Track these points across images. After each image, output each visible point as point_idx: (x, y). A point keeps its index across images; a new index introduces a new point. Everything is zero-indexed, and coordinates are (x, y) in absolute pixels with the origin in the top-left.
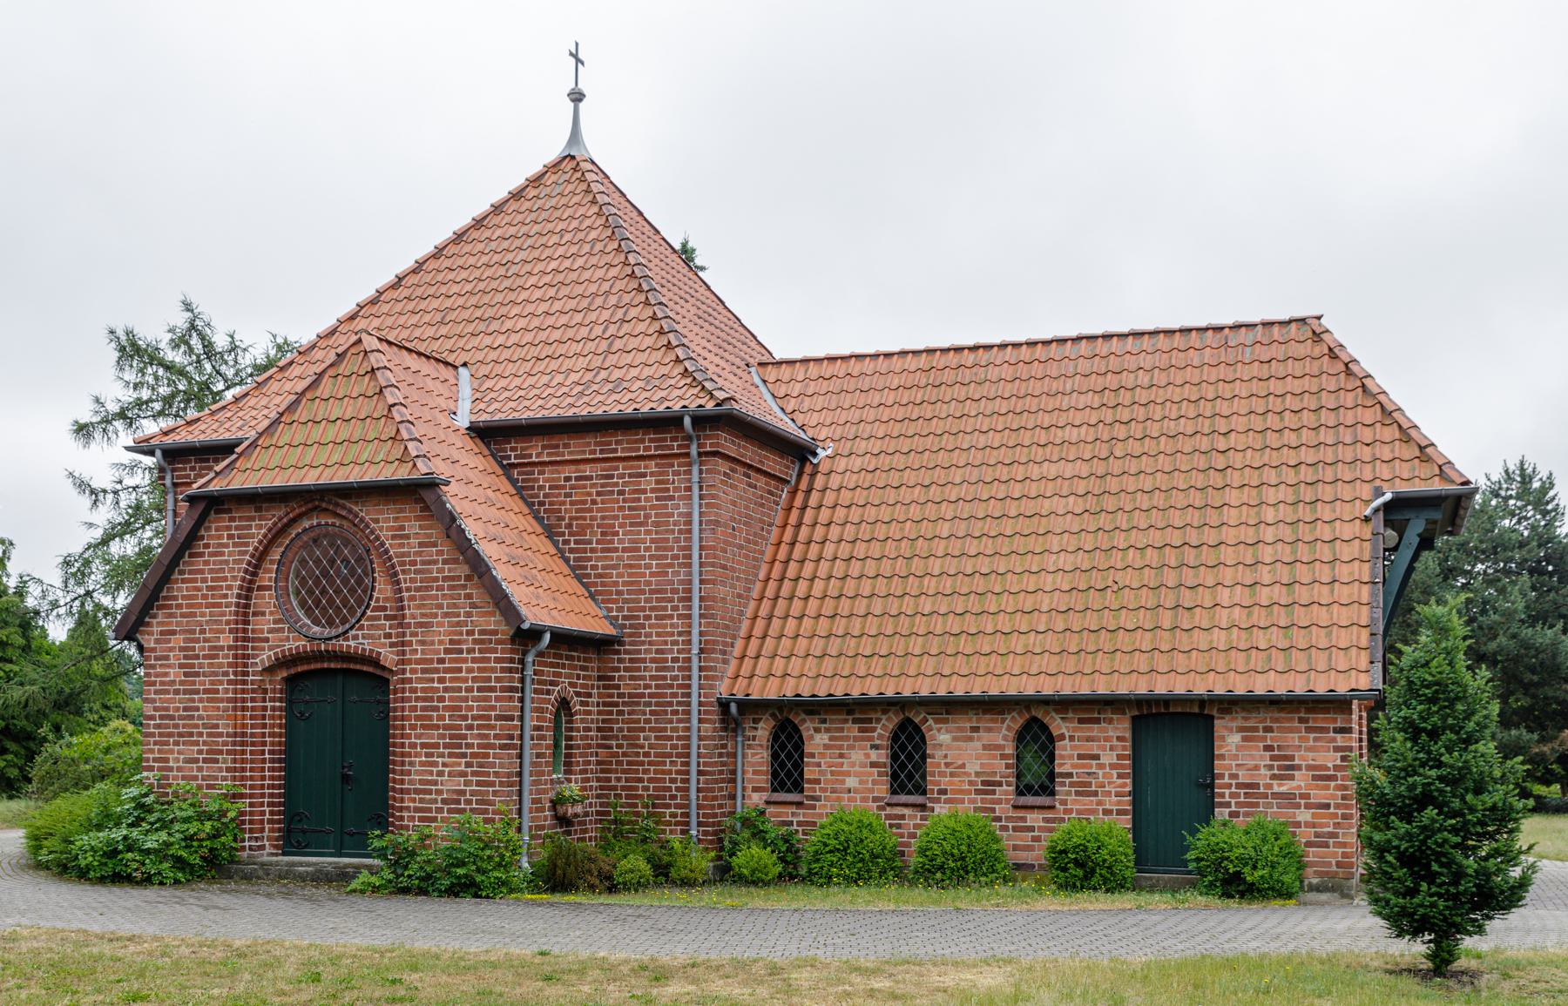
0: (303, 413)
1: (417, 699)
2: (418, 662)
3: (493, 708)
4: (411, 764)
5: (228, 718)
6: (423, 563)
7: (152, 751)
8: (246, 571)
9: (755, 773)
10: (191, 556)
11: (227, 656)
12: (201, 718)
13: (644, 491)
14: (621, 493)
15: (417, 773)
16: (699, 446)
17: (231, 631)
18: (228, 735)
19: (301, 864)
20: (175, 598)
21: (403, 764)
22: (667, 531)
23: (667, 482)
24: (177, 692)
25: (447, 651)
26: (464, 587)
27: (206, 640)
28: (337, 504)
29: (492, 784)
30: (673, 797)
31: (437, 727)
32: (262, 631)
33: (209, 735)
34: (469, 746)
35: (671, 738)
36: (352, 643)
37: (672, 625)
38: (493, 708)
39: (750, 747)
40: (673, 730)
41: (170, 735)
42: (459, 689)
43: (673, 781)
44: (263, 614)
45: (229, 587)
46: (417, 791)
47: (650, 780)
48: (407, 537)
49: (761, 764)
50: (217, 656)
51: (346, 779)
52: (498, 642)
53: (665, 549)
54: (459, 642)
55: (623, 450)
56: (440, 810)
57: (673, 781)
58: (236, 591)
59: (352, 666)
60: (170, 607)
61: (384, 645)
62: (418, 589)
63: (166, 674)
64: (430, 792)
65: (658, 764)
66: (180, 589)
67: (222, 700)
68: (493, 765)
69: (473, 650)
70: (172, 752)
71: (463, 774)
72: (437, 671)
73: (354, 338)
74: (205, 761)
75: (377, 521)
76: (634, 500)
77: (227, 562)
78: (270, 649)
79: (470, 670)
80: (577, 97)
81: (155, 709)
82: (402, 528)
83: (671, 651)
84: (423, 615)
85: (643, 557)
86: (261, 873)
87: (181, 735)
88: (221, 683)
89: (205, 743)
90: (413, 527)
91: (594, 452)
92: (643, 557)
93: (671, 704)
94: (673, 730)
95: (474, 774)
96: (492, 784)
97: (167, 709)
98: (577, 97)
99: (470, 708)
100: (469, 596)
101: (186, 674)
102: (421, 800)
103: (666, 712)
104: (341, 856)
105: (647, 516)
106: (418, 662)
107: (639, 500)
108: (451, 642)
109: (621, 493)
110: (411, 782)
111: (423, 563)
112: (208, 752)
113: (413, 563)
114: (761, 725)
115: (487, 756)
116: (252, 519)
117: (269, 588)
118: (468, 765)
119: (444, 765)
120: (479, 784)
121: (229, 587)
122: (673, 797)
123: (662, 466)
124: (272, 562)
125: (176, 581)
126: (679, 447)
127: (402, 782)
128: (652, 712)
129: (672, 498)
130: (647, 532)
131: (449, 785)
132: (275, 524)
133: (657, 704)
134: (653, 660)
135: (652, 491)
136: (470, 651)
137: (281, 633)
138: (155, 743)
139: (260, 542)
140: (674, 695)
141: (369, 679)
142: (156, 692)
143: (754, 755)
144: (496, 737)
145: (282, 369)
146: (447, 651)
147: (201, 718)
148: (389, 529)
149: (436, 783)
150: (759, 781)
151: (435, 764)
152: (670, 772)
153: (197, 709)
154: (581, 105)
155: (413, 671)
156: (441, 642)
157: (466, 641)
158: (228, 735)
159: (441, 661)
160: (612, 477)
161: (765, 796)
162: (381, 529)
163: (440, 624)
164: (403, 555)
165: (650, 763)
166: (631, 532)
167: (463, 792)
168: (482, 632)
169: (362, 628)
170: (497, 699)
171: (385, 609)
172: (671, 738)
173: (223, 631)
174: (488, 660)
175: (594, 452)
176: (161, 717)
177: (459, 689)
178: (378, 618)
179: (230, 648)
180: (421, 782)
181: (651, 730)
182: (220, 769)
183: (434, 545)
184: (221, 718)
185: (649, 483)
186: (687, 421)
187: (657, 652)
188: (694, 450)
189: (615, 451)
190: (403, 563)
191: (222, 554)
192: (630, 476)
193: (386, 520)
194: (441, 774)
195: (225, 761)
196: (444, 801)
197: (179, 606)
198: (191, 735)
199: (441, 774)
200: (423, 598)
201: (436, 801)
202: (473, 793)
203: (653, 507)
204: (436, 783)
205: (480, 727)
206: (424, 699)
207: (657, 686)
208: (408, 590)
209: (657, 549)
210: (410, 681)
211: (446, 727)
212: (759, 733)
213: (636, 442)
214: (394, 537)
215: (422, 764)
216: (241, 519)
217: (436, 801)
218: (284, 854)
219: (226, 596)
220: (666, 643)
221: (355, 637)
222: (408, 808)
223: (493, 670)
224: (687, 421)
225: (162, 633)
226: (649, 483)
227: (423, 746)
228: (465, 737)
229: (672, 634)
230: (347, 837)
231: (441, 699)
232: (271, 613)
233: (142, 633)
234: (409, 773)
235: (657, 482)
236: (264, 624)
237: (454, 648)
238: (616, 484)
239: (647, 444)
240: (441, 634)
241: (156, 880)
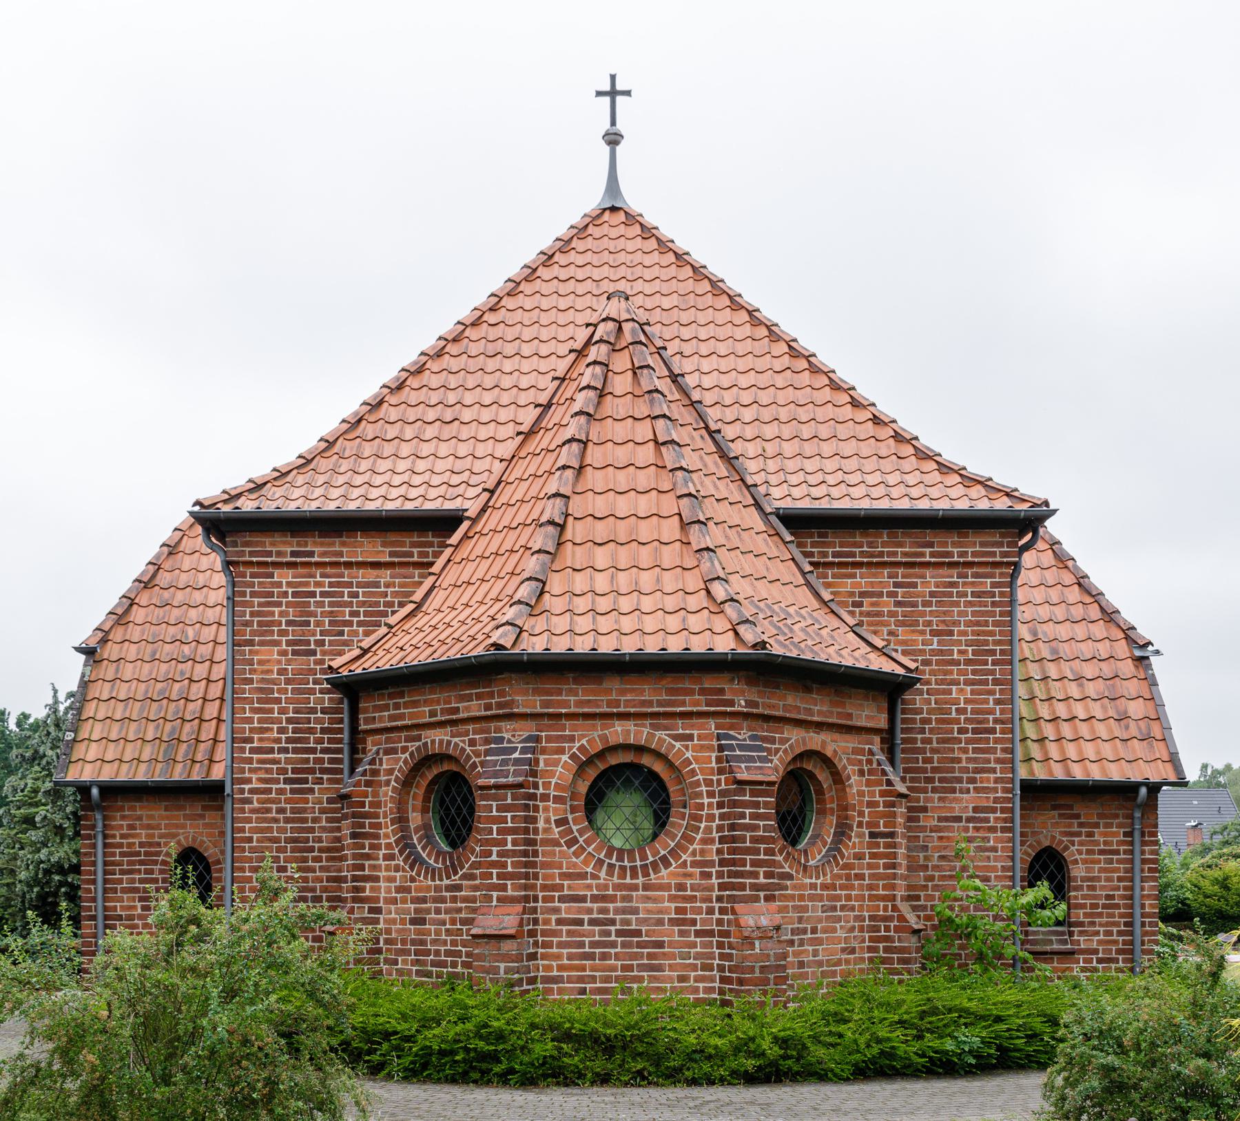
154: (618, 148)
239: (368, 548)
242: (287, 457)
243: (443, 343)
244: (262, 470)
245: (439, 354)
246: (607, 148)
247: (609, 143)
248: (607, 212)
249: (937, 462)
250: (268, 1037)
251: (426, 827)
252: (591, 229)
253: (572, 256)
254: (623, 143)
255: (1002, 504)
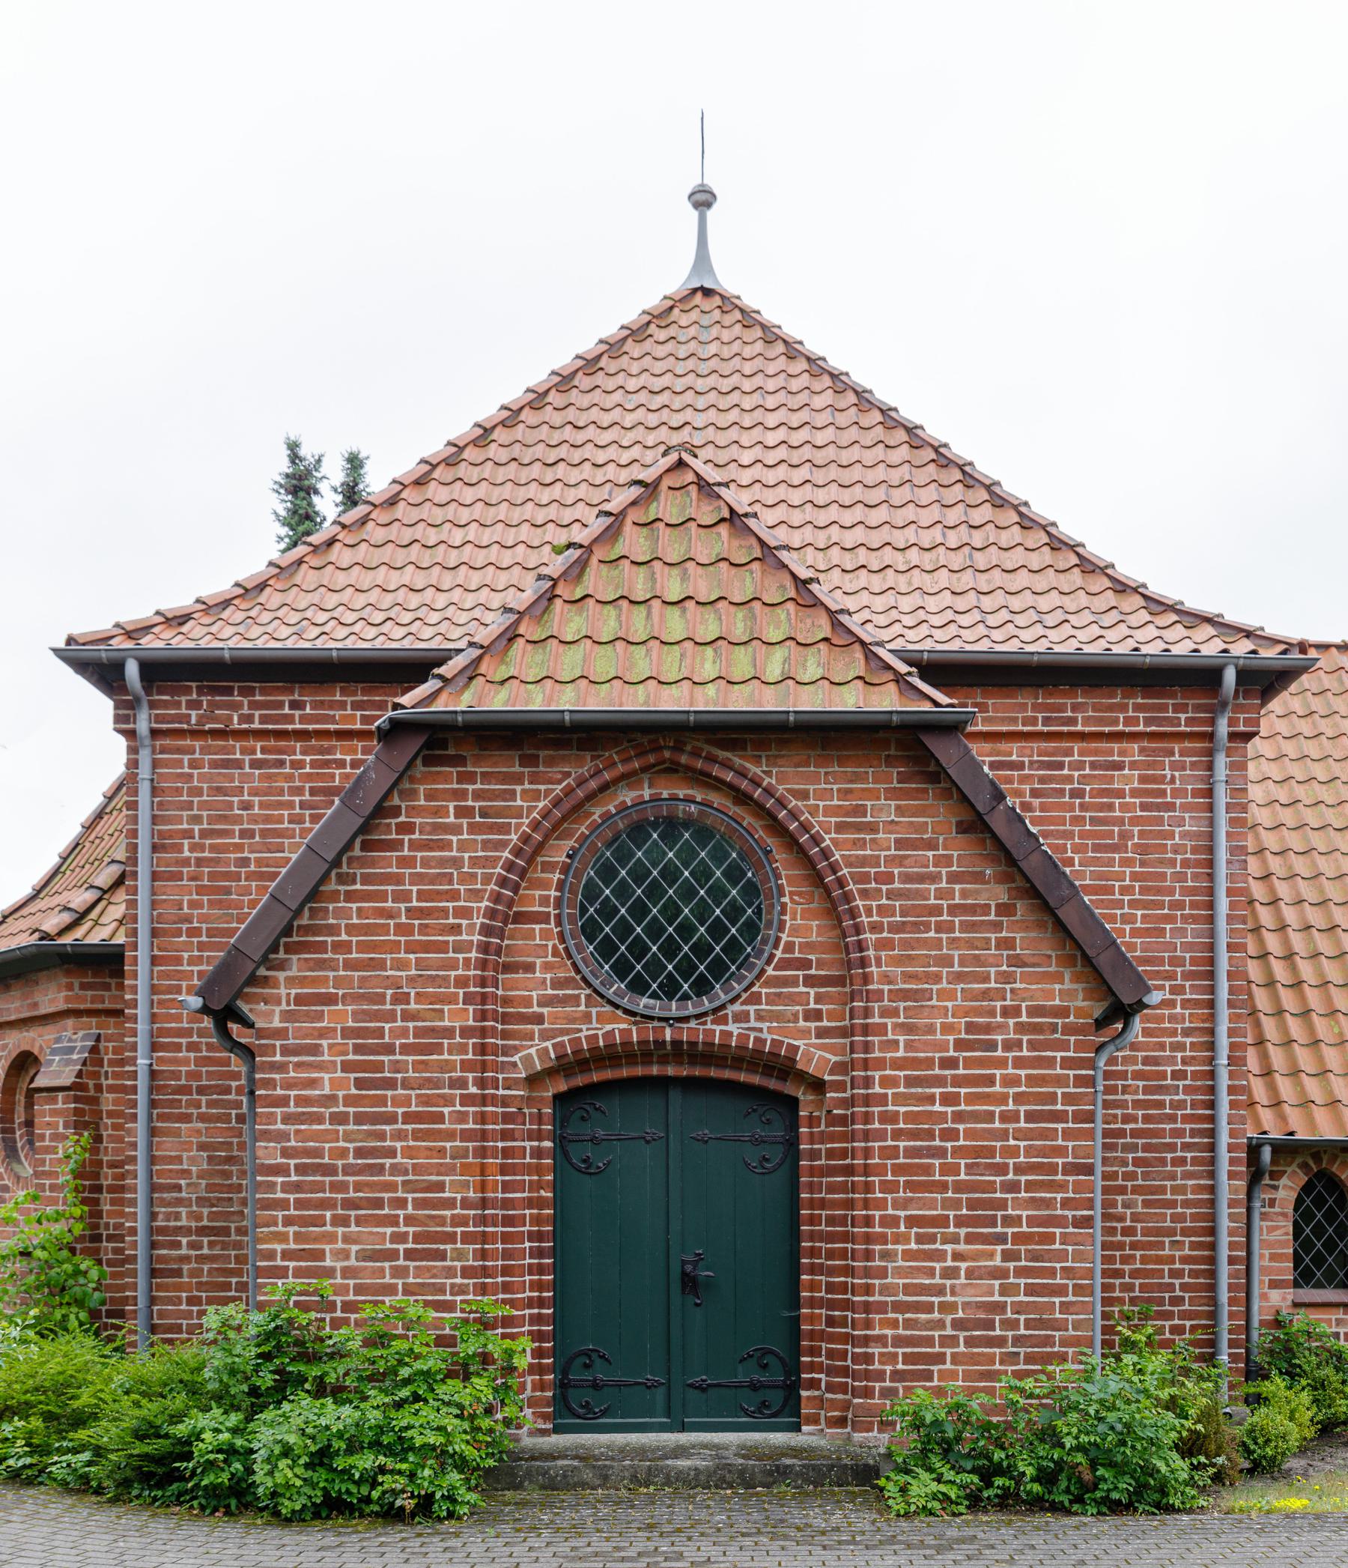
0: (597, 580)
1: (897, 1135)
2: (897, 1064)
3: (1061, 1151)
4: (886, 1255)
5: (466, 1169)
6: (907, 878)
7: (282, 1238)
8: (503, 882)
9: (1273, 1257)
10: (366, 846)
11: (462, 1049)
12: (396, 1169)
13: (1120, 793)
14: (1077, 793)
15: (899, 1272)
16: (1232, 722)
17: (468, 999)
18: (466, 1204)
19: (680, 1452)
20: (333, 930)
21: (868, 1255)
22: (1162, 862)
23: (1161, 779)
24: (340, 1119)
25: (960, 1045)
26: (997, 926)
27: (407, 1016)
28: (712, 759)
29: (1061, 1291)
30: (1176, 1301)
31: (943, 1187)
32: (527, 1002)
33: (419, 1204)
34: (1008, 1221)
35: (1172, 1204)
36: (734, 1028)
37: (1173, 1018)
38: (1061, 1151)
39: (1264, 1216)
40: (1175, 1190)
41: (324, 1204)
42: (989, 1117)
43: (1175, 1274)
44: (529, 968)
45: (464, 913)
46: (898, 1307)
47: (1135, 1274)
48: (872, 828)
49: (1282, 1244)
50: (437, 1049)
51: (690, 1283)
52: (1069, 1030)
53: (1159, 891)
54: (988, 1029)
55: (1087, 721)
56: (949, 1341)
57: (1175, 1274)
58: (479, 921)
59: (713, 1073)
60: (321, 947)
61: (805, 1033)
62: (895, 928)
63: (312, 1083)
64: (929, 1308)
65: (1150, 1246)
66: (344, 913)
67: (450, 1135)
68: (1062, 1256)
69: (1019, 1044)
70: (331, 1238)
71: (1000, 1273)
72: (940, 1081)
73: (673, 457)
74: (410, 1255)
75: (804, 795)
76: (1102, 807)
77: (457, 863)
78: (545, 1036)
79: (1010, 1081)
80: (703, 200)
81: (286, 1153)
82: (861, 811)
83: (1172, 1060)
84: (908, 977)
85: (1120, 904)
86: (588, 1475)
87: (349, 1204)
88: (448, 1101)
89: (409, 1220)
90: (884, 810)
91: (1034, 721)
92: (1120, 904)
93: (1172, 1147)
94: (1175, 1190)
95: (1020, 1272)
96: (1061, 1291)
97: (317, 1153)
98: (703, 200)
99: (1014, 1152)
100: (1006, 944)
101: (360, 1084)
102: (909, 1324)
103: (1163, 1162)
104: (683, 1428)
105: (1125, 836)
106: (897, 1064)
107: (1110, 807)
108: (970, 1028)
109: (1077, 793)
110: (885, 1290)
111: (907, 878)
112: (418, 1238)
113: (888, 878)
114: (1284, 1181)
115: (1050, 1239)
116: (518, 779)
117: (544, 918)
118: (1007, 1256)
119: (958, 1256)
120: (1031, 1290)
121: (464, 913)
122: (1176, 1301)
123: (1154, 752)
124: (548, 867)
125: (334, 896)
126: (1190, 721)
127: (868, 1290)
128: (1137, 1162)
129: (1171, 807)
130: (1125, 862)
131: (966, 1294)
132: (569, 792)
133: (1147, 1148)
134: (1138, 1075)
135: (1135, 793)
136: (1008, 1046)
137: (567, 1011)
138: (288, 1221)
139: (535, 826)
140: (1178, 1133)
141: (766, 1092)
142: (287, 1119)
143: (1271, 1229)
144: (1066, 1203)
145: (316, 549)
146: (960, 1045)
147: (396, 1169)
148: (829, 811)
149: (940, 1291)
150: (1280, 1271)
151: (940, 1256)
152: (1171, 1260)
153: (391, 1153)
154: (710, 214)
155: (886, 1082)
156: (947, 1029)
157: (1002, 1028)
158: (466, 1204)
159: (950, 1063)
160: (1060, 766)
161: (1290, 1294)
162: (814, 811)
163: (943, 995)
164: (864, 861)
165: (1134, 1246)
166: (1095, 861)
167: (1000, 1307)
168: (1033, 1011)
169: (755, 999)
170: (1067, 1134)
171: (806, 964)
172: (1172, 1204)
173: (451, 999)
174: (1050, 1062)
175: (1034, 721)
176: (301, 1169)
177: (989, 1117)
178: (793, 982)
179: (466, 1032)
180: (908, 1289)
181: (1136, 1190)
182: (450, 1272)
183: (931, 845)
184: (450, 1170)
185: (1128, 779)
186: (1230, 676)
187: (1146, 1061)
188: (1223, 728)
189: (1073, 721)
190: (864, 878)
191: (446, 845)
192: (1094, 766)
193: (822, 795)
194: (950, 1273)
195: (462, 1255)
196: (958, 1324)
197: (341, 947)
198: (378, 1204)
199: (950, 1273)
200: (906, 944)
201: (940, 1324)
202: (1018, 1308)
203: (1134, 821)
204: (940, 1291)
205: (1030, 1186)
206: (914, 1135)
207: (1147, 1119)
208: (876, 928)
209: (1143, 890)
210: (882, 1100)
211: (959, 1187)
212: (1281, 1194)
213: (1111, 708)
214: (840, 827)
215: (908, 1255)
216: (486, 777)
217: (940, 1324)
218: (557, 1430)
219: (456, 929)
220: (1162, 1046)
221: (742, 1017)
222: (881, 1340)
223: (1060, 1081)
224: (1230, 676)
225: (299, 1000)
226: (1128, 779)
227: (912, 1221)
228: (1002, 1205)
229: (1173, 1033)
230: (693, 1394)
231: (950, 1135)
232: (547, 967)
233: (250, 999)
234: (882, 1273)
235: (1143, 779)
236: (534, 988)
237: (977, 1039)
238: (1069, 779)
239: (1131, 712)
240: (947, 1013)
241: (441, 1508)
242: (220, 585)
243: (399, 487)
244: (180, 600)
245: (420, 482)
246: (695, 214)
247: (697, 205)
248: (699, 295)
249: (1144, 596)
250: (44, 1222)
251: (990, 1459)
252: (629, 346)
253: (599, 378)
254: (715, 206)
255: (1184, 645)
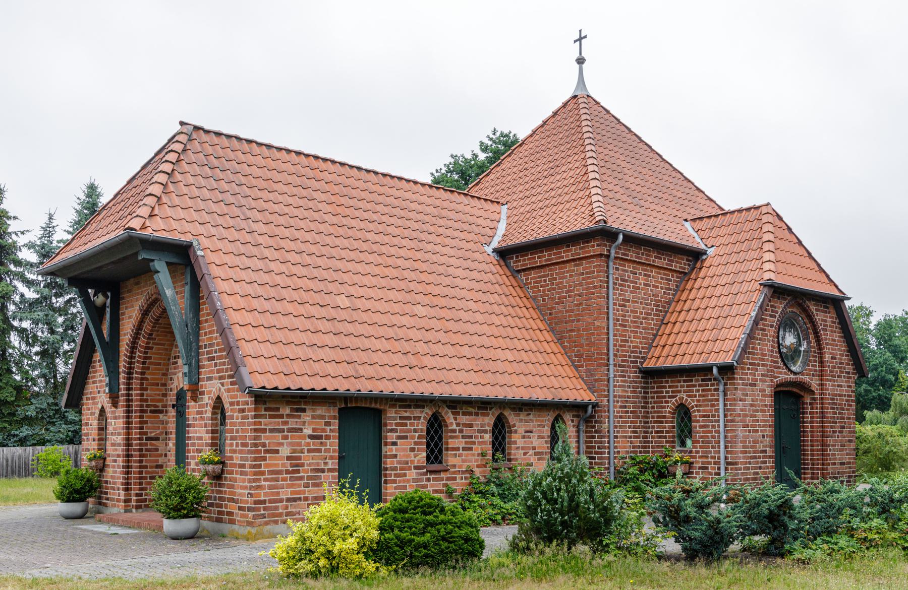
154: (577, 55)
